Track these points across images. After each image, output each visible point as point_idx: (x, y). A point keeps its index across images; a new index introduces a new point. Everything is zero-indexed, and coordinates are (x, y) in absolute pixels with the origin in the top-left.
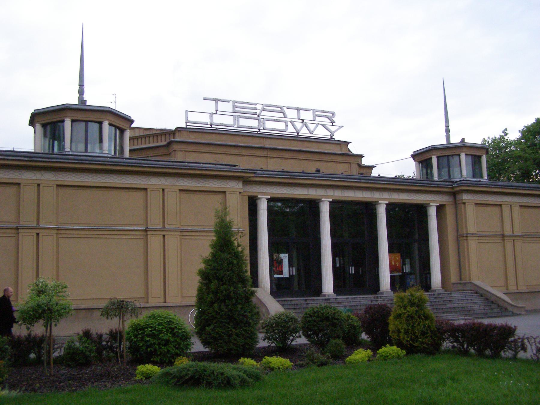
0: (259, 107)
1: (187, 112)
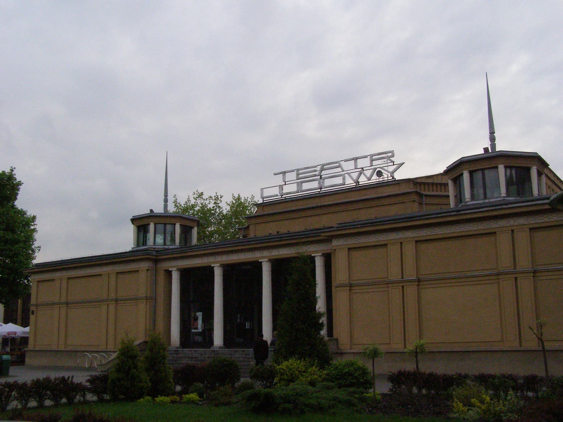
0: (318, 168)
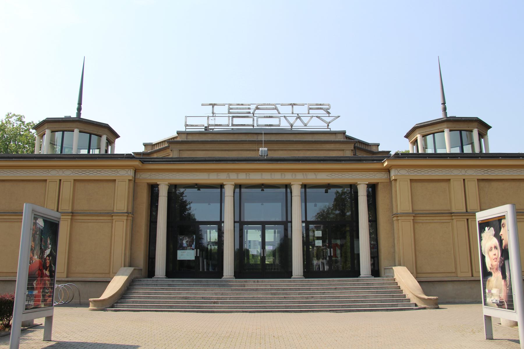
0: (253, 107)
1: (186, 117)
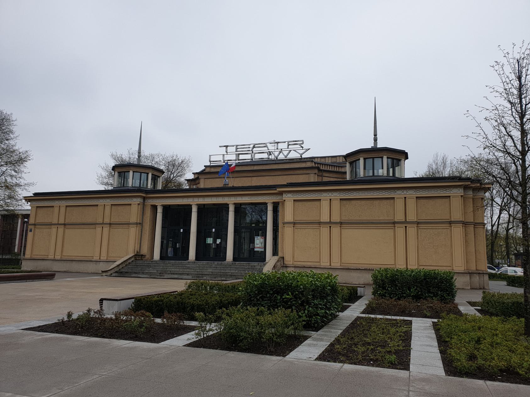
0: (252, 146)
1: (210, 156)
